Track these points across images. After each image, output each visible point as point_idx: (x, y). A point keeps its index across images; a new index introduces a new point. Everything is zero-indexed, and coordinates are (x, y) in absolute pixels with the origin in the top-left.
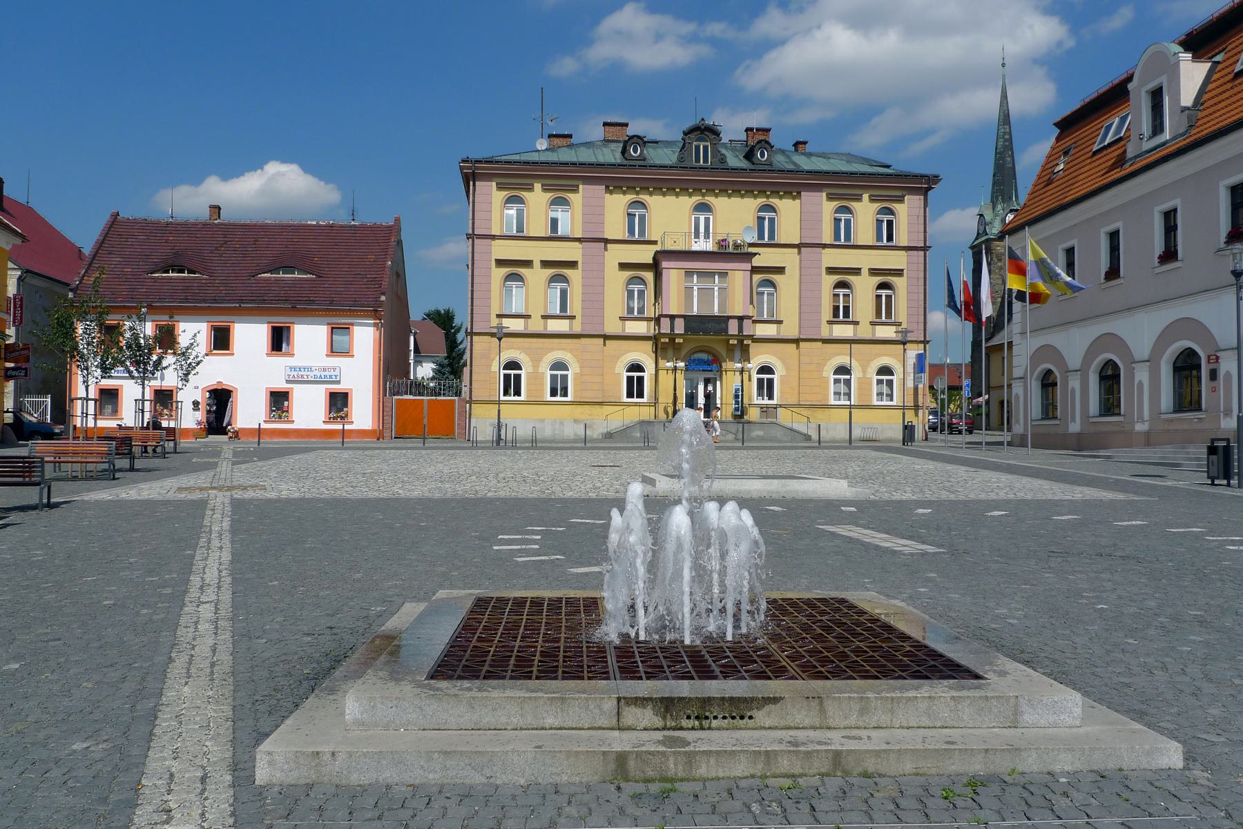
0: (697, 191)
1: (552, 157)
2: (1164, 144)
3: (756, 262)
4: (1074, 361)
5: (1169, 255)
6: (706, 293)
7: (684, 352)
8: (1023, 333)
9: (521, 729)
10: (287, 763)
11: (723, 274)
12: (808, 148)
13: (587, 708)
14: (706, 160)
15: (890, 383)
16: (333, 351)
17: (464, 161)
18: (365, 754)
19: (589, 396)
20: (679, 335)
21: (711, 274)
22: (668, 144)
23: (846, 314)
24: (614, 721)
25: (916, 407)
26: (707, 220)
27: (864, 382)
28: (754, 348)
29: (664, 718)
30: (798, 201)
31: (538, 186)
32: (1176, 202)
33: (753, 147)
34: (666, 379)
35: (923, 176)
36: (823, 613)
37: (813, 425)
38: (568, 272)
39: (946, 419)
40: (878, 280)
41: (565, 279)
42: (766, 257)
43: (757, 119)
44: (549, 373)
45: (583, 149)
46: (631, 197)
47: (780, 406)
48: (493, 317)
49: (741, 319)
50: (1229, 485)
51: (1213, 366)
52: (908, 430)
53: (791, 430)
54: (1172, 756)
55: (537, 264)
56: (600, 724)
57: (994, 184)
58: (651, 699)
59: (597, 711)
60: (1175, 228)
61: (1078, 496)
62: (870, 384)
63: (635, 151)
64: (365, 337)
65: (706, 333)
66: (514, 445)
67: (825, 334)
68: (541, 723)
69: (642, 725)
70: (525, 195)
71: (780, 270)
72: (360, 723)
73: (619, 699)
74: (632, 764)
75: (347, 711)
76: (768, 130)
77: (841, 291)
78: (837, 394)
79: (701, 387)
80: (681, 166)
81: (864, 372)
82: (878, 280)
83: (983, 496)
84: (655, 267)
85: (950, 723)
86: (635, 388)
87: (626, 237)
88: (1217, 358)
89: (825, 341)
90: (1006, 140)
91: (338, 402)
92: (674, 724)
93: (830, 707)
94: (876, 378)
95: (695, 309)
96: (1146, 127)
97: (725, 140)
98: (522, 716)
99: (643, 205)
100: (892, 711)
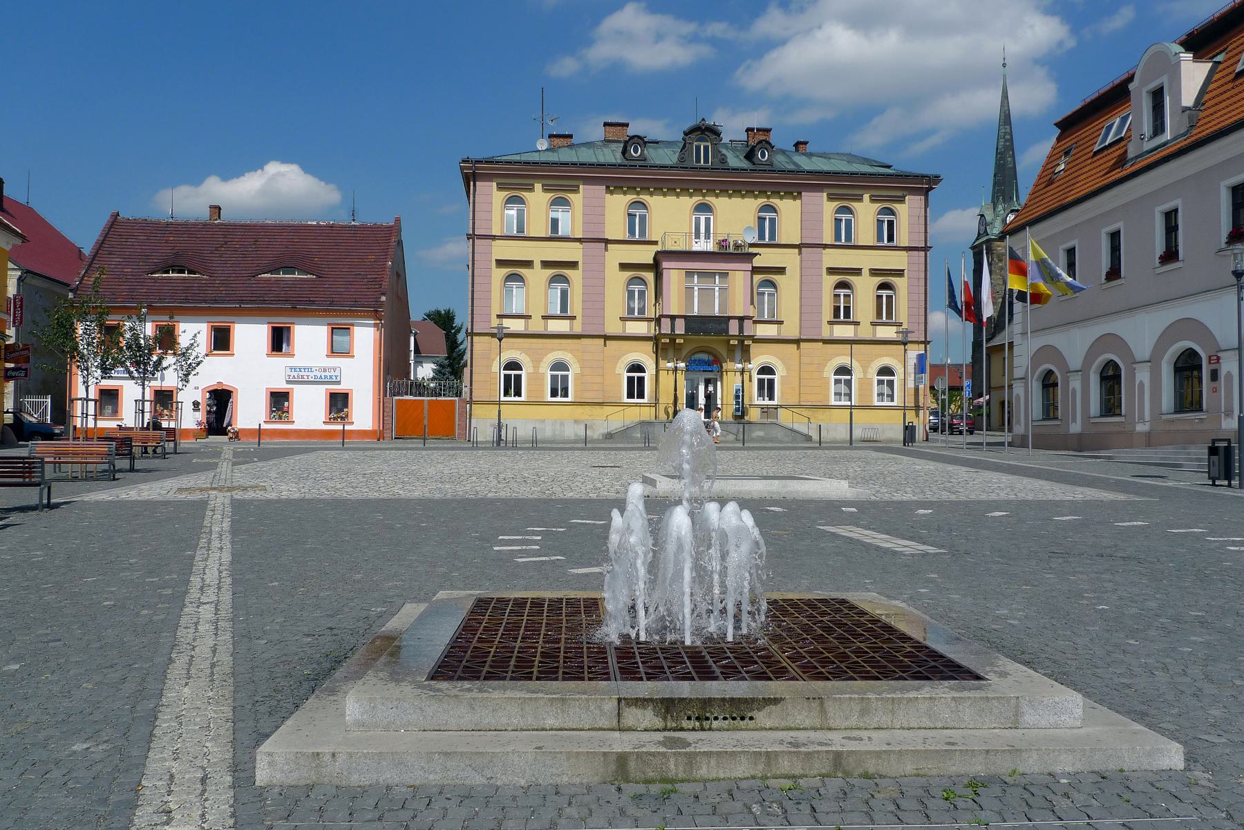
1: (552, 157)
2: (1165, 144)
3: (757, 262)
4: (1075, 361)
5: (1170, 255)
9: (522, 730)
10: (287, 763)
12: (809, 148)
18: (365, 756)
23: (847, 315)
26: (708, 220)
28: (754, 349)
30: (798, 202)
32: (1177, 203)
34: (667, 379)
35: (923, 176)
41: (565, 279)
42: (766, 258)
48: (494, 317)
49: (741, 319)
50: (1230, 485)
51: (1214, 367)
54: (1173, 756)
55: (537, 264)
58: (651, 700)
59: (597, 712)
60: (1176, 228)
62: (828, 383)
63: (636, 152)
67: (826, 334)
69: (643, 726)
73: (619, 700)
74: (632, 765)
77: (842, 292)
79: (702, 388)
84: (655, 267)
86: (635, 388)
87: (627, 237)
88: (1218, 358)
89: (826, 342)
90: (1006, 141)
95: (696, 309)
96: (1147, 128)
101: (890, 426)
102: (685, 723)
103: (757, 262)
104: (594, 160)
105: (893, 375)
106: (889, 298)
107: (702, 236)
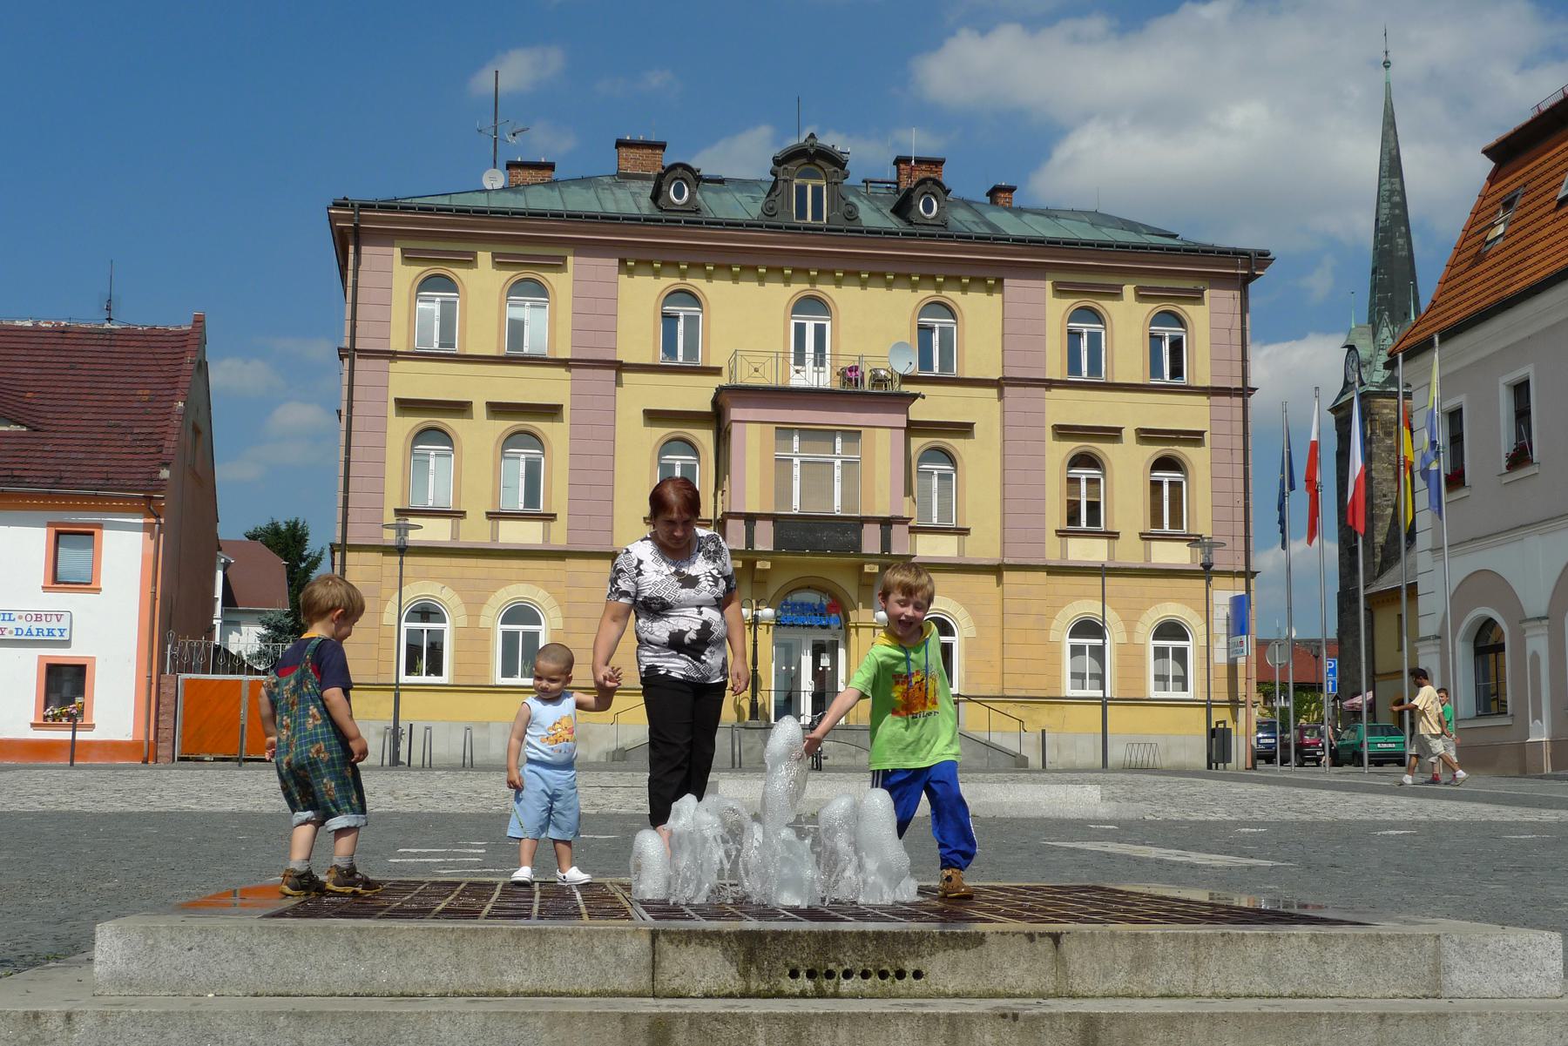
0: (801, 273)
3: (918, 412)
6: (817, 472)
7: (772, 590)
8: (1436, 550)
11: (852, 435)
13: (590, 953)
14: (817, 214)
15: (1181, 655)
16: (57, 580)
17: (337, 205)
20: (764, 554)
21: (827, 434)
22: (744, 185)
24: (644, 981)
25: (1234, 703)
26: (820, 331)
27: (1130, 652)
29: (745, 974)
30: (997, 297)
31: (484, 257)
33: (910, 191)
35: (1237, 253)
37: (1032, 738)
38: (541, 426)
39: (1292, 736)
40: (1154, 451)
41: (535, 440)
42: (934, 404)
43: (917, 143)
44: (500, 628)
46: (668, 282)
47: (969, 699)
49: (886, 523)
52: (1219, 740)
53: (987, 745)
55: (479, 410)
56: (615, 984)
57: (1375, 287)
61: (1553, 818)
62: (1142, 656)
63: (679, 194)
64: (125, 552)
65: (817, 550)
67: (1052, 556)
68: (496, 983)
70: (460, 273)
71: (964, 430)
72: (122, 981)
75: (98, 957)
76: (938, 163)
77: (1083, 473)
78: (1078, 676)
79: (807, 661)
80: (769, 223)
81: (1130, 632)
82: (1154, 451)
83: (1367, 817)
84: (716, 419)
85: (1310, 988)
87: (660, 358)
89: (1053, 570)
91: (65, 684)
92: (764, 986)
95: (796, 503)
97: (854, 179)
98: (458, 967)
99: (693, 298)
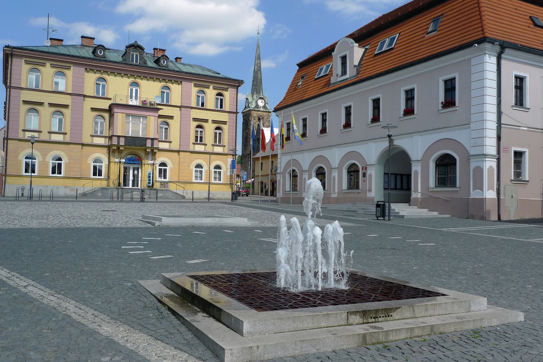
1: (52, 50)
2: (346, 79)
3: (161, 113)
5: (347, 125)
9: (313, 329)
10: (239, 353)
12: (182, 61)
15: (201, 172)
18: (270, 345)
19: (72, 175)
23: (201, 140)
26: (136, 91)
28: (158, 154)
30: (180, 86)
32: (352, 104)
34: (115, 167)
35: (237, 80)
36: (224, 279)
37: (190, 192)
40: (216, 125)
41: (62, 113)
42: (165, 111)
45: (71, 48)
46: (98, 75)
48: (20, 131)
49: (153, 139)
50: (384, 219)
51: (364, 171)
53: (176, 193)
54: (521, 317)
55: (46, 104)
58: (359, 311)
59: (340, 318)
60: (350, 114)
62: (192, 172)
63: (101, 53)
66: (40, 198)
67: (191, 149)
69: (355, 323)
73: (348, 313)
74: (368, 337)
77: (199, 130)
79: (131, 172)
82: (216, 125)
84: (110, 110)
86: (97, 171)
87: (95, 95)
88: (366, 168)
89: (192, 152)
90: (258, 67)
93: (416, 309)
94: (194, 169)
95: (130, 134)
96: (339, 72)
100: (434, 309)
101: (226, 193)
102: (370, 320)
103: (161, 113)
104: (78, 54)
105: (62, 160)
106: (220, 134)
107: (134, 98)
